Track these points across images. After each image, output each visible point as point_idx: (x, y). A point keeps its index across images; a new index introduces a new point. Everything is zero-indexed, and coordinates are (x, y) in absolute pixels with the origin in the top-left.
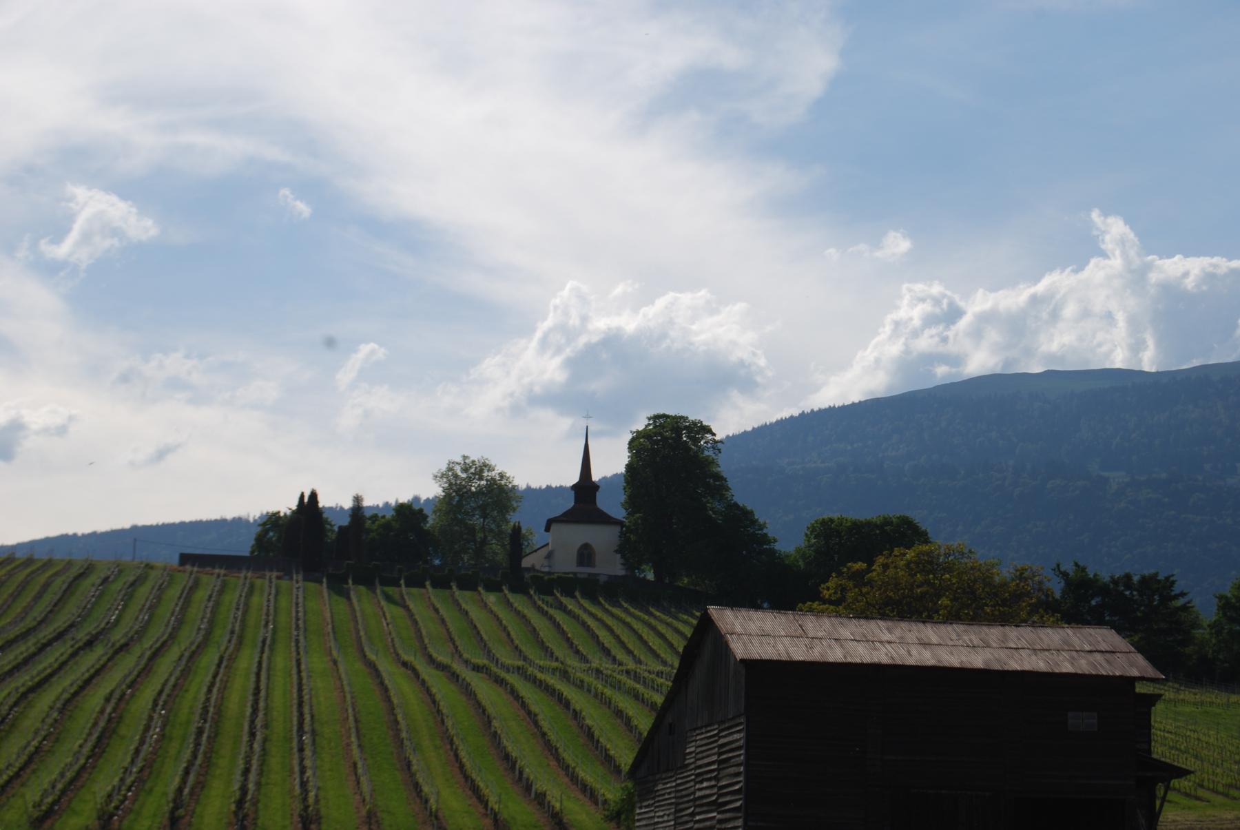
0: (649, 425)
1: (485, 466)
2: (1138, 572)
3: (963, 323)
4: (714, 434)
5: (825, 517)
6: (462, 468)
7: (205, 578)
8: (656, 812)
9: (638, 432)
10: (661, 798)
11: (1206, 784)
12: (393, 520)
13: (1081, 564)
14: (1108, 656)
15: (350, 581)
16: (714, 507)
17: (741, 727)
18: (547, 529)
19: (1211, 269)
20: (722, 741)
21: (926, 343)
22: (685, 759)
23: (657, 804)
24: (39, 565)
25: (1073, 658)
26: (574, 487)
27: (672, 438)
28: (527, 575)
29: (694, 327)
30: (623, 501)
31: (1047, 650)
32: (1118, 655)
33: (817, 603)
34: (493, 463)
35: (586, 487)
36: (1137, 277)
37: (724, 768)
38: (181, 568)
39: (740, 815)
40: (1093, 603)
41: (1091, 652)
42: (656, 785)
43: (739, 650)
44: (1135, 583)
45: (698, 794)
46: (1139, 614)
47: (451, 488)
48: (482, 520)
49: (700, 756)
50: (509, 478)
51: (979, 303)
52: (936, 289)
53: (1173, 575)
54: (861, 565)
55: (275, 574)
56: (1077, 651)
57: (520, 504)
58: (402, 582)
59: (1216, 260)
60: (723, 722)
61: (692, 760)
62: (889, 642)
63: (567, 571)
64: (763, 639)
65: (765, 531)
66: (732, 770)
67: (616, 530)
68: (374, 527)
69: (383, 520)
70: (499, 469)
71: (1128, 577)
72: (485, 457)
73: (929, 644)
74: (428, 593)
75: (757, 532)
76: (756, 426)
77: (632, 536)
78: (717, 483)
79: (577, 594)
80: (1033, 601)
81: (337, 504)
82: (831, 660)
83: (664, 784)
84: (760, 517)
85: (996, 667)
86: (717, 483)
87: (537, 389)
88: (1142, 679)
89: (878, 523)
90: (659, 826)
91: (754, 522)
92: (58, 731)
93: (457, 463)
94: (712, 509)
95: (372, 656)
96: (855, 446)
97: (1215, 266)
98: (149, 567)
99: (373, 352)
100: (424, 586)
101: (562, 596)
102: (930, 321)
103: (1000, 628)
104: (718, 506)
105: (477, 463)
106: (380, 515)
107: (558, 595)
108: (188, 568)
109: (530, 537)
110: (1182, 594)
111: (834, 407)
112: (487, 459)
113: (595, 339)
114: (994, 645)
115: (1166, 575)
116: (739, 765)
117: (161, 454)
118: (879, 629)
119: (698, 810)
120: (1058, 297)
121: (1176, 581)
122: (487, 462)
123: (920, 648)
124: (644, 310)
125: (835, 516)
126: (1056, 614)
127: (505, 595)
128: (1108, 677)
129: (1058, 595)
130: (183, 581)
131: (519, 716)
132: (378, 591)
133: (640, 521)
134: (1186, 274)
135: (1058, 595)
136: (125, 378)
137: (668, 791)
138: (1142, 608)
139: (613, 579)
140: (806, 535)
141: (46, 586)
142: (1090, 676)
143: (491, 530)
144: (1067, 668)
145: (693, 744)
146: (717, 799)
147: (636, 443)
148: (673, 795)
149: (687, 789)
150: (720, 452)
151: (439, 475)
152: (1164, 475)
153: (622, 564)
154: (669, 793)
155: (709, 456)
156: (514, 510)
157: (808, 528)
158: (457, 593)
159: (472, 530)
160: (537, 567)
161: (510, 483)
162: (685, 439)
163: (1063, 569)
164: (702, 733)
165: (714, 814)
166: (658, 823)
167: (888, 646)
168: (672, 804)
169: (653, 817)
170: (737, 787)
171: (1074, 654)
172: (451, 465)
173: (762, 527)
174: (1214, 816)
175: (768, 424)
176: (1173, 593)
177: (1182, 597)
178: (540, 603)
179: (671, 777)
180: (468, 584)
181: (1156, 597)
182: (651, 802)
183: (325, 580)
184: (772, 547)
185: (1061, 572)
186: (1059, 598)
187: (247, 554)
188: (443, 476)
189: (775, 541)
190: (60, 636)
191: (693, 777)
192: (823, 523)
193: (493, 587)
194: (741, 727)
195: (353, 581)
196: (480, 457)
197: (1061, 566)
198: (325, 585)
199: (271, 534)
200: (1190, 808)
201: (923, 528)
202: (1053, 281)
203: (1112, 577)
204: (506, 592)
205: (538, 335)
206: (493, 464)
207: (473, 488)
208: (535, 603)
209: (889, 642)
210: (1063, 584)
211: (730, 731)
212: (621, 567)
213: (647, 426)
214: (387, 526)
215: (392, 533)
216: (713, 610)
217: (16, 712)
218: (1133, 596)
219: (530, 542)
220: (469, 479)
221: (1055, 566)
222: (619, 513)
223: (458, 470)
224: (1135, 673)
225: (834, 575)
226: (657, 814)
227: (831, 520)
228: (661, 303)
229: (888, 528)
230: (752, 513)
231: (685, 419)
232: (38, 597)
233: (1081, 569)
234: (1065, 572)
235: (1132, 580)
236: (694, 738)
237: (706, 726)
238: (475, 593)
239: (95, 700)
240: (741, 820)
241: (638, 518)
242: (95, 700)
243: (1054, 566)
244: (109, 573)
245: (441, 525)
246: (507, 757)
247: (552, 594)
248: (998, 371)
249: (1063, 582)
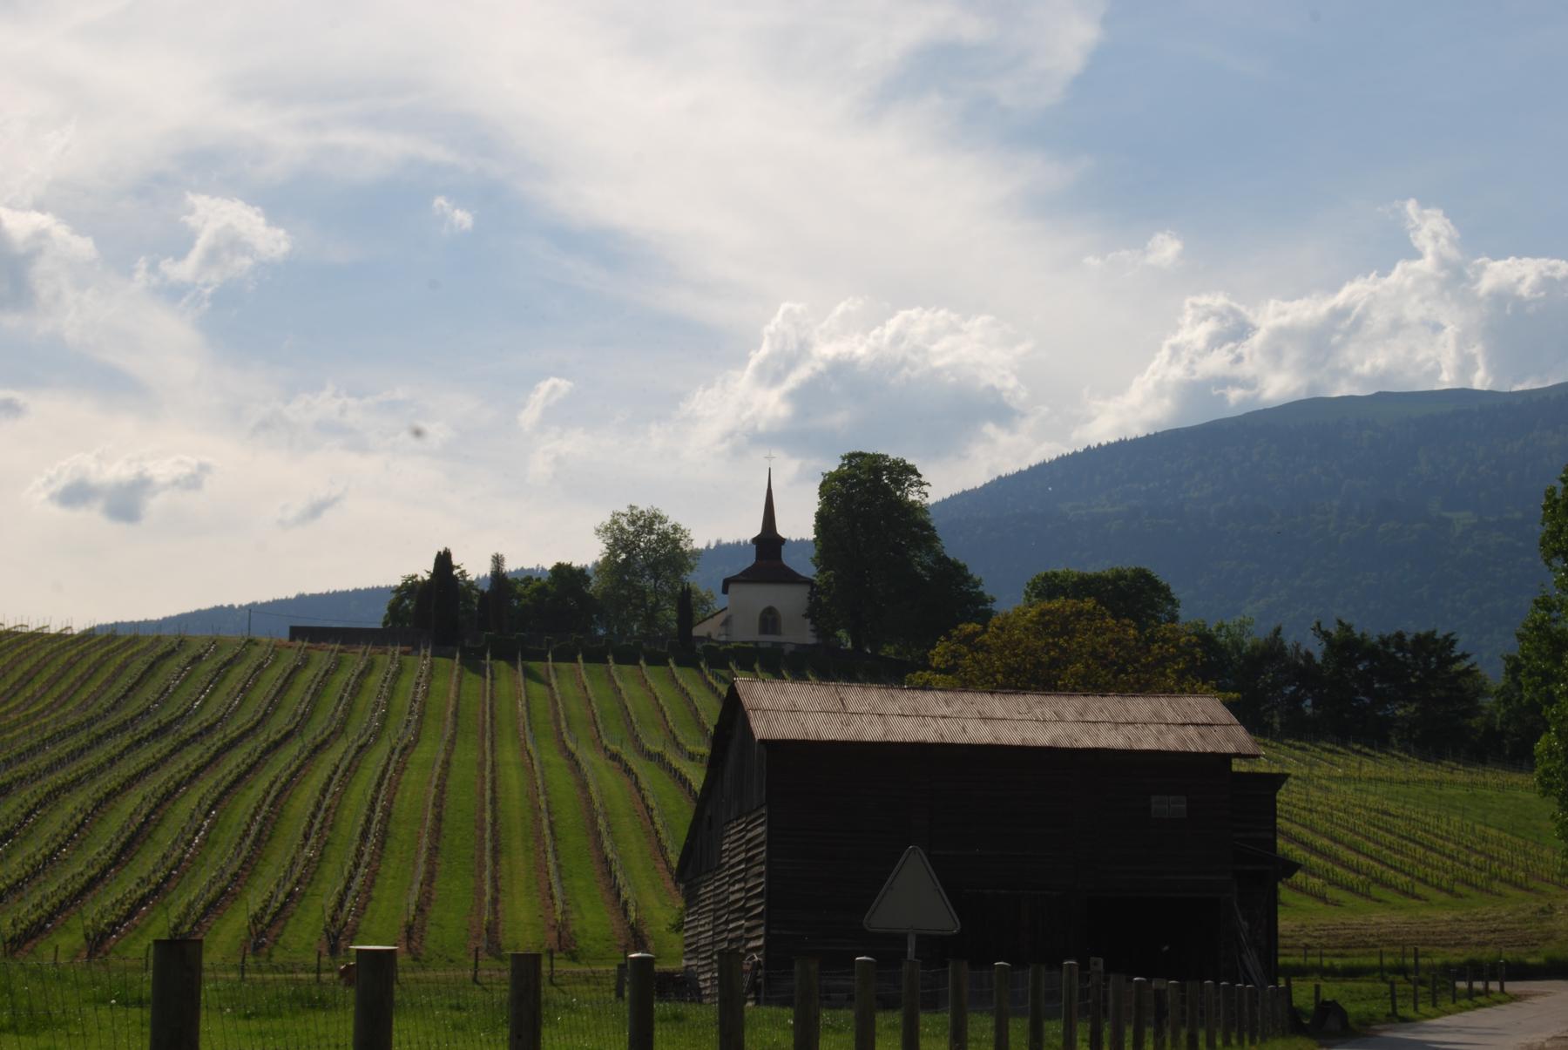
0: (843, 465)
1: (655, 518)
2: (1413, 628)
3: (1257, 340)
4: (919, 476)
5: (1049, 571)
6: (628, 521)
7: (380, 659)
8: (699, 920)
9: (830, 474)
10: (703, 904)
11: (1429, 879)
12: (550, 583)
13: (1346, 621)
14: (1203, 729)
15: (488, 656)
16: (921, 561)
17: (762, 820)
18: (725, 591)
19: (1548, 273)
20: (750, 835)
21: (1217, 362)
22: (722, 858)
23: (700, 911)
24: (122, 641)
25: (1161, 732)
26: (755, 540)
27: (871, 481)
28: (699, 646)
29: (935, 348)
30: (813, 556)
31: (1131, 723)
32: (1216, 728)
33: (929, 672)
34: (664, 513)
35: (769, 541)
36: (1455, 278)
37: (752, 867)
38: (290, 644)
39: (762, 922)
40: (1361, 668)
41: (1184, 724)
42: (699, 890)
43: (761, 729)
44: (1409, 643)
45: (732, 898)
46: (1413, 680)
47: (617, 545)
48: (653, 581)
49: (732, 854)
50: (684, 531)
51: (1272, 315)
52: (1219, 301)
53: (1452, 634)
54: (974, 627)
55: (398, 649)
56: (1168, 724)
57: (697, 562)
58: (550, 656)
59: (1553, 262)
60: (749, 814)
61: (727, 859)
62: (944, 717)
63: (747, 640)
64: (792, 715)
65: (981, 589)
66: (756, 870)
67: (806, 590)
68: (527, 592)
69: (538, 583)
70: (672, 521)
71: (1400, 636)
72: (655, 507)
73: (992, 719)
74: (580, 668)
75: (971, 590)
78: (926, 533)
79: (757, 666)
80: (1180, 666)
81: (538, 565)
82: (868, 738)
83: (706, 887)
84: (975, 571)
85: (1065, 743)
86: (926, 533)
87: (761, 427)
88: (1238, 755)
89: (1110, 577)
90: (703, 936)
91: (968, 578)
92: (82, 836)
93: (623, 515)
94: (920, 564)
95: (571, 746)
96: (1151, 485)
97: (1553, 269)
98: (251, 642)
99: (554, 388)
100: (575, 660)
101: (737, 669)
102: (1216, 341)
103: (1082, 698)
104: (928, 560)
105: (646, 514)
106: (534, 578)
107: (734, 668)
108: (299, 643)
109: (710, 600)
110: (1464, 656)
111: (1126, 439)
112: (657, 509)
113: (820, 366)
114: (1070, 718)
115: (1445, 633)
116: (761, 863)
117: (316, 510)
118: (997, 705)
119: (731, 917)
120: (1357, 310)
121: (1457, 640)
122: (657, 512)
123: (980, 724)
124: (877, 331)
125: (1060, 570)
126: (1211, 682)
127: (671, 669)
128: (1197, 754)
129: (1318, 658)
130: (289, 659)
131: (636, 811)
132: (520, 667)
133: (832, 580)
134: (1521, 280)
135: (1318, 658)
136: (264, 425)
137: (708, 895)
138: (1418, 673)
140: (1026, 593)
141: (124, 666)
142: (1176, 754)
143: (664, 593)
144: (1149, 744)
145: (727, 840)
146: (745, 904)
147: (827, 487)
148: (712, 900)
149: (723, 892)
150: (927, 496)
151: (603, 529)
152: (1518, 515)
153: (812, 630)
154: (709, 898)
155: (914, 502)
156: (692, 569)
157: (1028, 584)
158: (677, 671)
159: (641, 593)
160: (714, 637)
161: (686, 536)
162: (886, 481)
163: (1323, 629)
164: (733, 828)
165: (743, 922)
166: (701, 933)
167: (941, 722)
168: (710, 911)
169: (696, 927)
170: (759, 890)
171: (1163, 727)
172: (616, 517)
173: (977, 584)
174: (1428, 917)
175: (1047, 461)
176: (1453, 655)
177: (1464, 659)
178: (710, 678)
179: (711, 879)
180: (627, 657)
181: (1433, 659)
182: (696, 908)
183: (458, 655)
184: (989, 607)
185: (1322, 632)
186: (1320, 662)
187: (380, 626)
188: (607, 529)
189: (993, 600)
190: (123, 727)
191: (727, 879)
192: (1046, 578)
193: (656, 660)
194: (762, 820)
195: (491, 656)
196: (649, 507)
197: (1322, 624)
198: (457, 660)
199: (407, 602)
200: (1401, 908)
201: (1164, 583)
202: (1353, 292)
203: (1380, 637)
204: (672, 665)
205: (753, 363)
206: (665, 515)
207: (642, 544)
208: (705, 678)
209: (944, 717)
211: (755, 824)
212: (811, 634)
213: (841, 467)
214: (542, 590)
215: (547, 599)
216: (742, 681)
217: (38, 815)
218: (1406, 659)
219: (711, 606)
220: (637, 534)
221: (1314, 625)
222: (808, 570)
223: (624, 522)
224: (1231, 748)
225: (942, 638)
226: (701, 923)
227: (1055, 575)
228: (892, 325)
229: (1122, 583)
230: (964, 567)
231: (885, 457)
232: (110, 681)
233: (1347, 628)
234: (1327, 632)
235: (1404, 640)
236: (727, 834)
237: (737, 819)
238: (636, 667)
239: (132, 802)
240: (763, 928)
241: (830, 576)
242: (132, 802)
243: (1314, 625)
244: (202, 651)
245: (605, 588)
246: (606, 861)
247: (727, 667)
248: (1303, 396)
249: (1325, 644)
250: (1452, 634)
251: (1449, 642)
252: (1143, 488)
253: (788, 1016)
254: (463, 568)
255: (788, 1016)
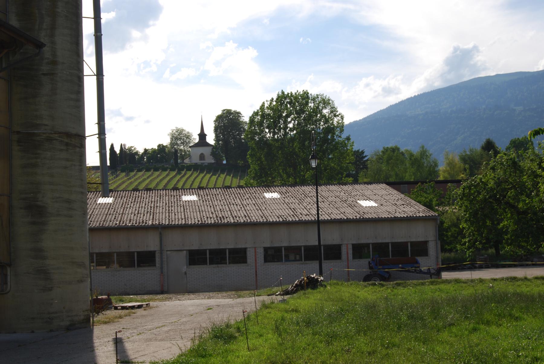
1: (183, 130)
53: (364, 150)
76: (400, 101)
77: (146, 159)
115: (362, 150)
139: (210, 164)
210: (201, 174)
250: (364, 150)
251: (363, 152)
252: (430, 106)
253: (318, 262)
254: (135, 147)
255: (318, 262)
